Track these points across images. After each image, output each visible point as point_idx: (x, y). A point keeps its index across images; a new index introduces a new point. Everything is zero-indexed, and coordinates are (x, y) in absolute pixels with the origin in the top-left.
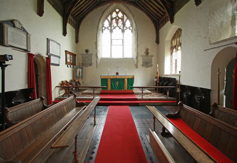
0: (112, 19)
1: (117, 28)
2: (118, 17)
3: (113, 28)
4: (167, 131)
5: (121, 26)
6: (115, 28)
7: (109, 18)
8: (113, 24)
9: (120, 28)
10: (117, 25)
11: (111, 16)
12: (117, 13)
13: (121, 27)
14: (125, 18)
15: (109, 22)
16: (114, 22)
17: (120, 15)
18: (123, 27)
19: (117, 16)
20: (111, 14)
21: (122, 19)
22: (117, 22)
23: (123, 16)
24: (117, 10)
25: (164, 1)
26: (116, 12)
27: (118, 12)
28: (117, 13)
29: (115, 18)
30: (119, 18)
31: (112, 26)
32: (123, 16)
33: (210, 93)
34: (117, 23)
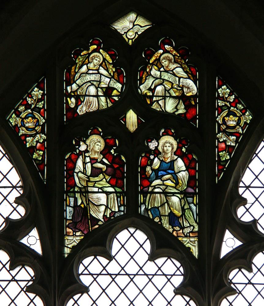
0: (66, 130)
1: (131, 244)
2: (142, 104)
3: (72, 240)
4: (262, 182)
5: (173, 219)
6: (99, 241)
7: (29, 122)
8: (85, 192)
9: (163, 244)
10: (131, 206)
11: (56, 97)
12: (130, 61)
13: (176, 231)
14: (232, 122)
15: (29, 160)
16: (96, 172)
17: (169, 82)
18: (210, 238)
19: (132, 98)
20: (56, 72)
21: (195, 130)
22: (133, 163)
23: (207, 94)
24: (130, 26)
25: (199, 305)
26: (113, 43)
27: (147, 42)
28: (130, 61)
29: (107, 121)
30: (155, 122)
31: (69, 212)
32: (207, 94)
33: (243, 197)
34: (129, 170)
